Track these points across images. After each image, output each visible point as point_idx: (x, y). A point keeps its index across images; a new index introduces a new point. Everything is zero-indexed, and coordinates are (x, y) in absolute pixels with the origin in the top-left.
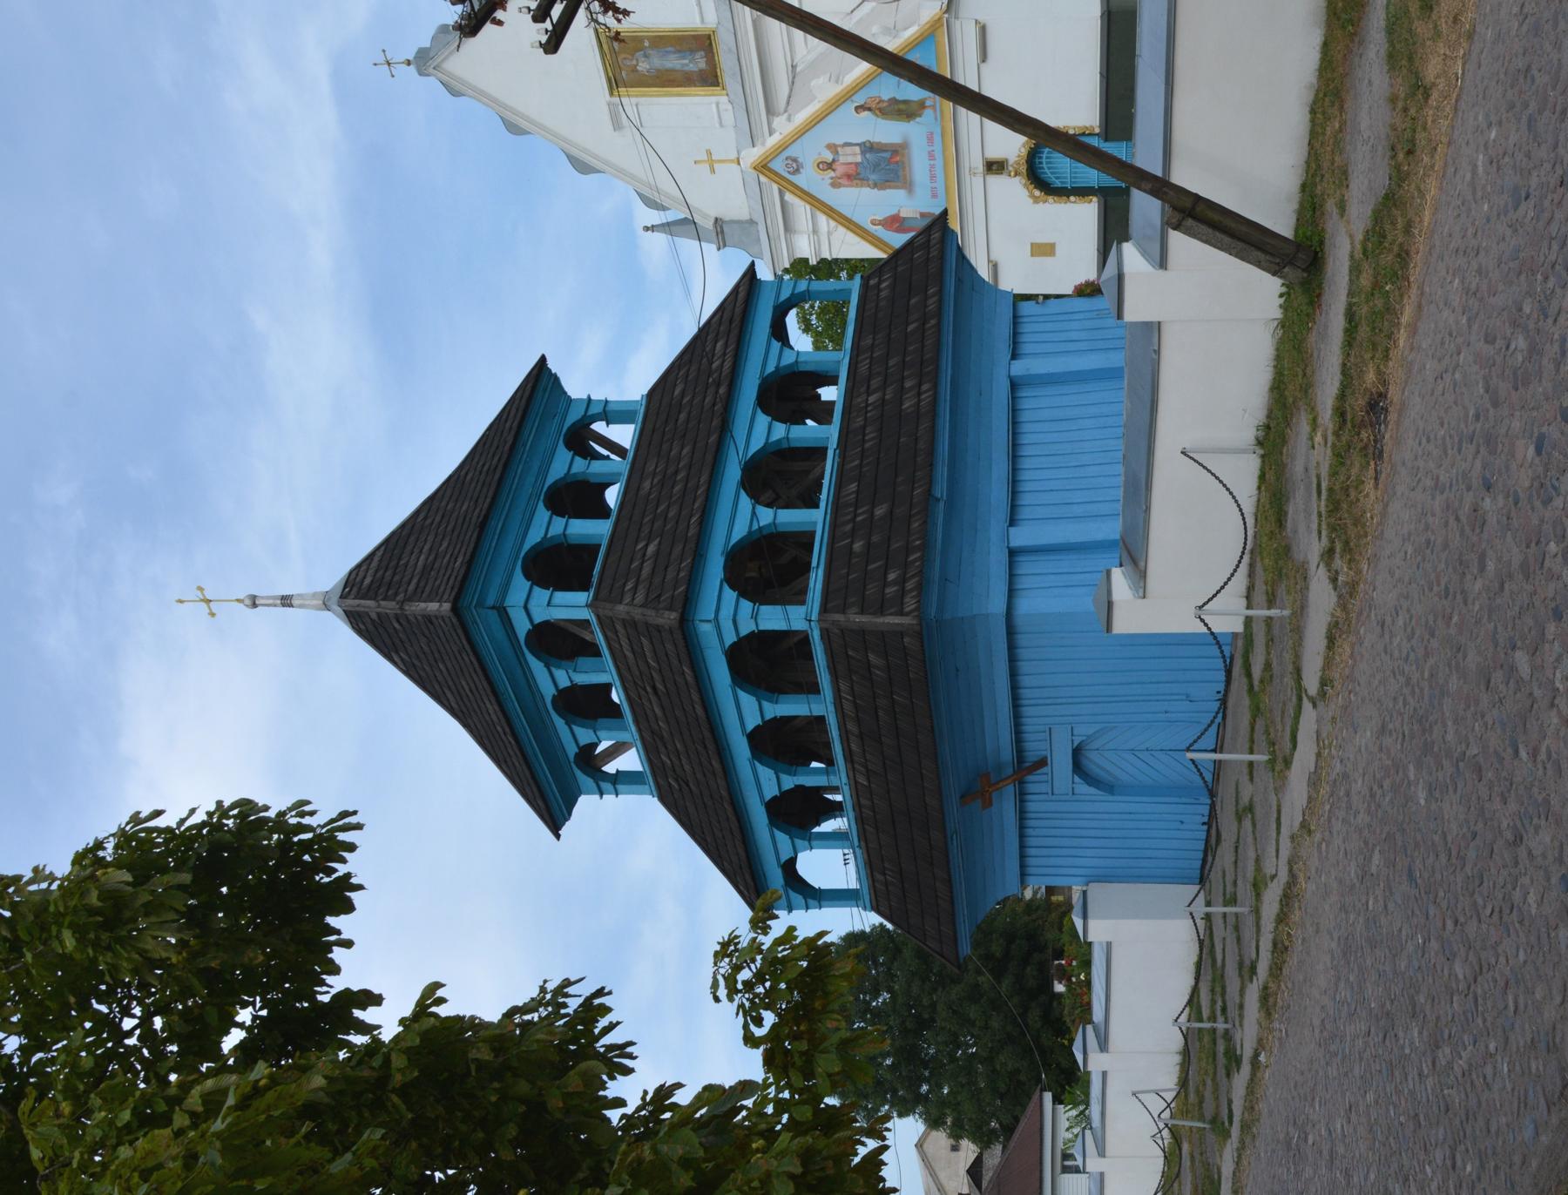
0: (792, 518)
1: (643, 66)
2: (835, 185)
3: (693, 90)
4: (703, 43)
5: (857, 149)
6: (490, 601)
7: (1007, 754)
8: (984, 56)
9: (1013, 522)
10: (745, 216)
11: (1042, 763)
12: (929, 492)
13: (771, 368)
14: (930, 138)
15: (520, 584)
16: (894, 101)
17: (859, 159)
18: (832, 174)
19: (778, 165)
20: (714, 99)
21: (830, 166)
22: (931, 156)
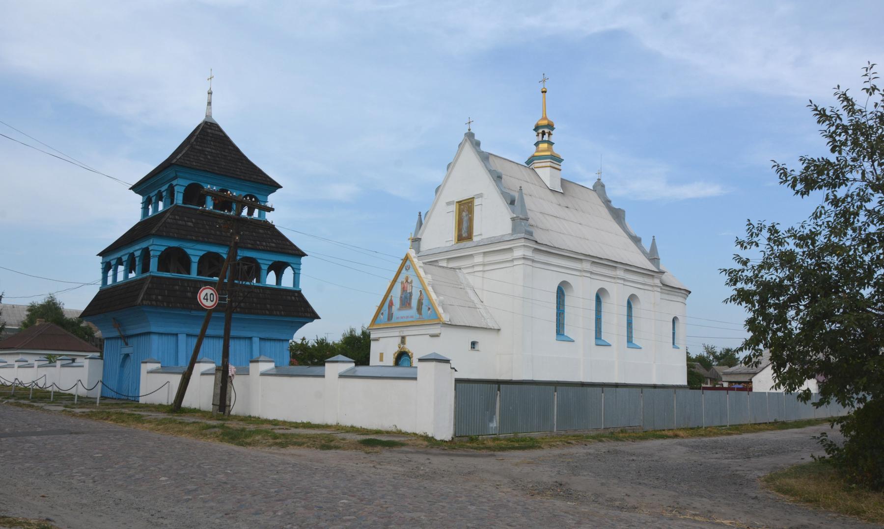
0: (194, 267)
1: (464, 214)
2: (402, 283)
4: (469, 237)
6: (179, 174)
7: (129, 333)
8: (432, 336)
9: (188, 335)
10: (422, 249)
11: (127, 344)
12: (192, 309)
13: (260, 261)
14: (412, 317)
15: (186, 183)
19: (408, 263)
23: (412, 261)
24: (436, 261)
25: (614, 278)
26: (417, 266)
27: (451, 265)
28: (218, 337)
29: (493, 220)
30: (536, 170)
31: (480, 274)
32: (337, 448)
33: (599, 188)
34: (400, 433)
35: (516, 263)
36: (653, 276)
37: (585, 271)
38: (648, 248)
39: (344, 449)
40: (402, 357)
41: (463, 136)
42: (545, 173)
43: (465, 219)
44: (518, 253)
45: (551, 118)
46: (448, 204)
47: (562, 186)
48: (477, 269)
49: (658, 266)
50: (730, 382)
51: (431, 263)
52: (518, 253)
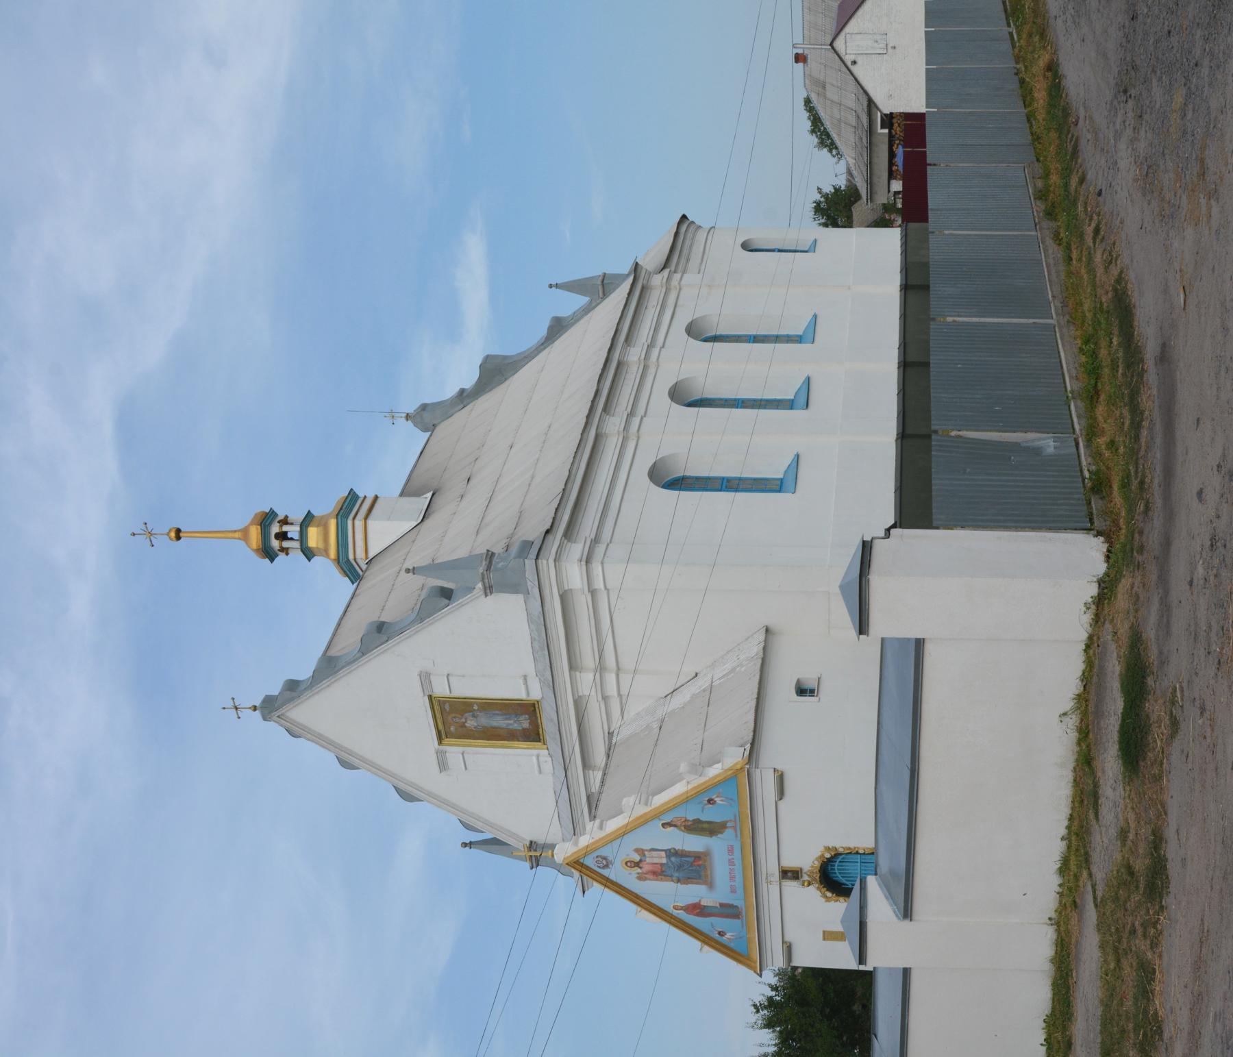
1: (471, 723)
3: (516, 743)
4: (530, 709)
5: (663, 854)
8: (781, 793)
14: (731, 850)
16: (697, 821)
17: (664, 861)
18: (639, 870)
19: (590, 861)
20: (535, 752)
22: (731, 862)
23: (588, 851)
24: (588, 798)
25: (646, 367)
26: (599, 835)
27: (599, 756)
29: (488, 648)
30: (371, 554)
31: (625, 679)
32: (1157, 841)
33: (427, 417)
34: (1087, 702)
35: (599, 584)
36: (644, 288)
37: (626, 427)
38: (582, 300)
39: (1163, 811)
40: (833, 877)
41: (271, 725)
42: (381, 532)
43: (484, 721)
44: (574, 576)
45: (243, 516)
46: (443, 765)
47: (418, 493)
48: (611, 689)
49: (617, 280)
50: (891, 175)
51: (593, 802)
52: (574, 576)
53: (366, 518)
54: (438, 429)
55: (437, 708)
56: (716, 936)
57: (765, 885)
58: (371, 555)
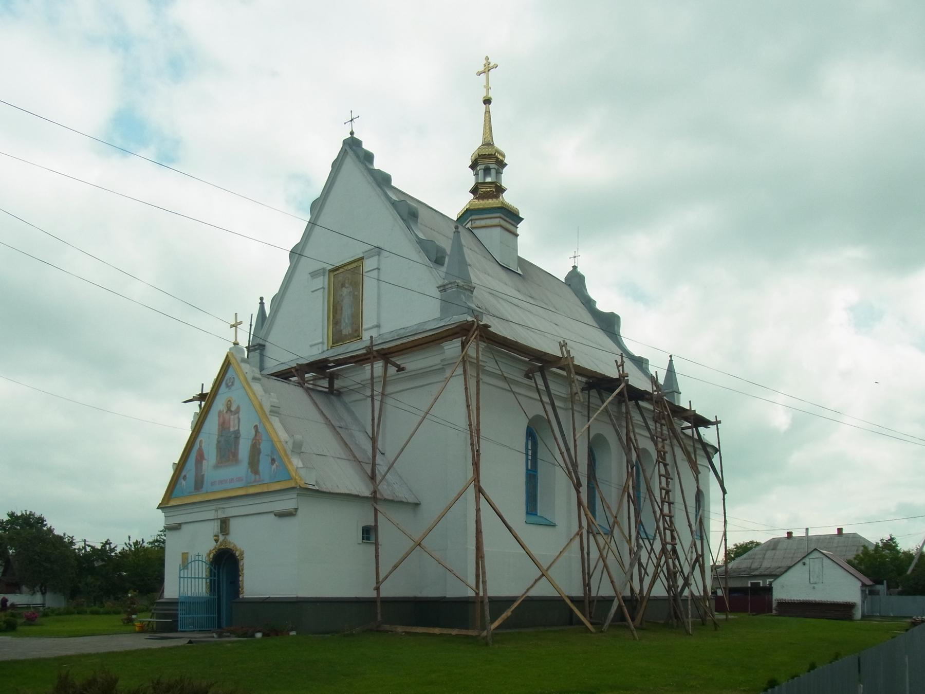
5: (236, 428)
8: (281, 515)
14: (240, 479)
16: (259, 452)
17: (232, 429)
21: (229, 409)
22: (232, 481)
28: (587, 586)
33: (575, 280)
43: (347, 302)
46: (314, 275)
53: (501, 226)
54: (567, 287)
55: (354, 265)
56: (183, 474)
57: (214, 508)
58: (474, 231)
